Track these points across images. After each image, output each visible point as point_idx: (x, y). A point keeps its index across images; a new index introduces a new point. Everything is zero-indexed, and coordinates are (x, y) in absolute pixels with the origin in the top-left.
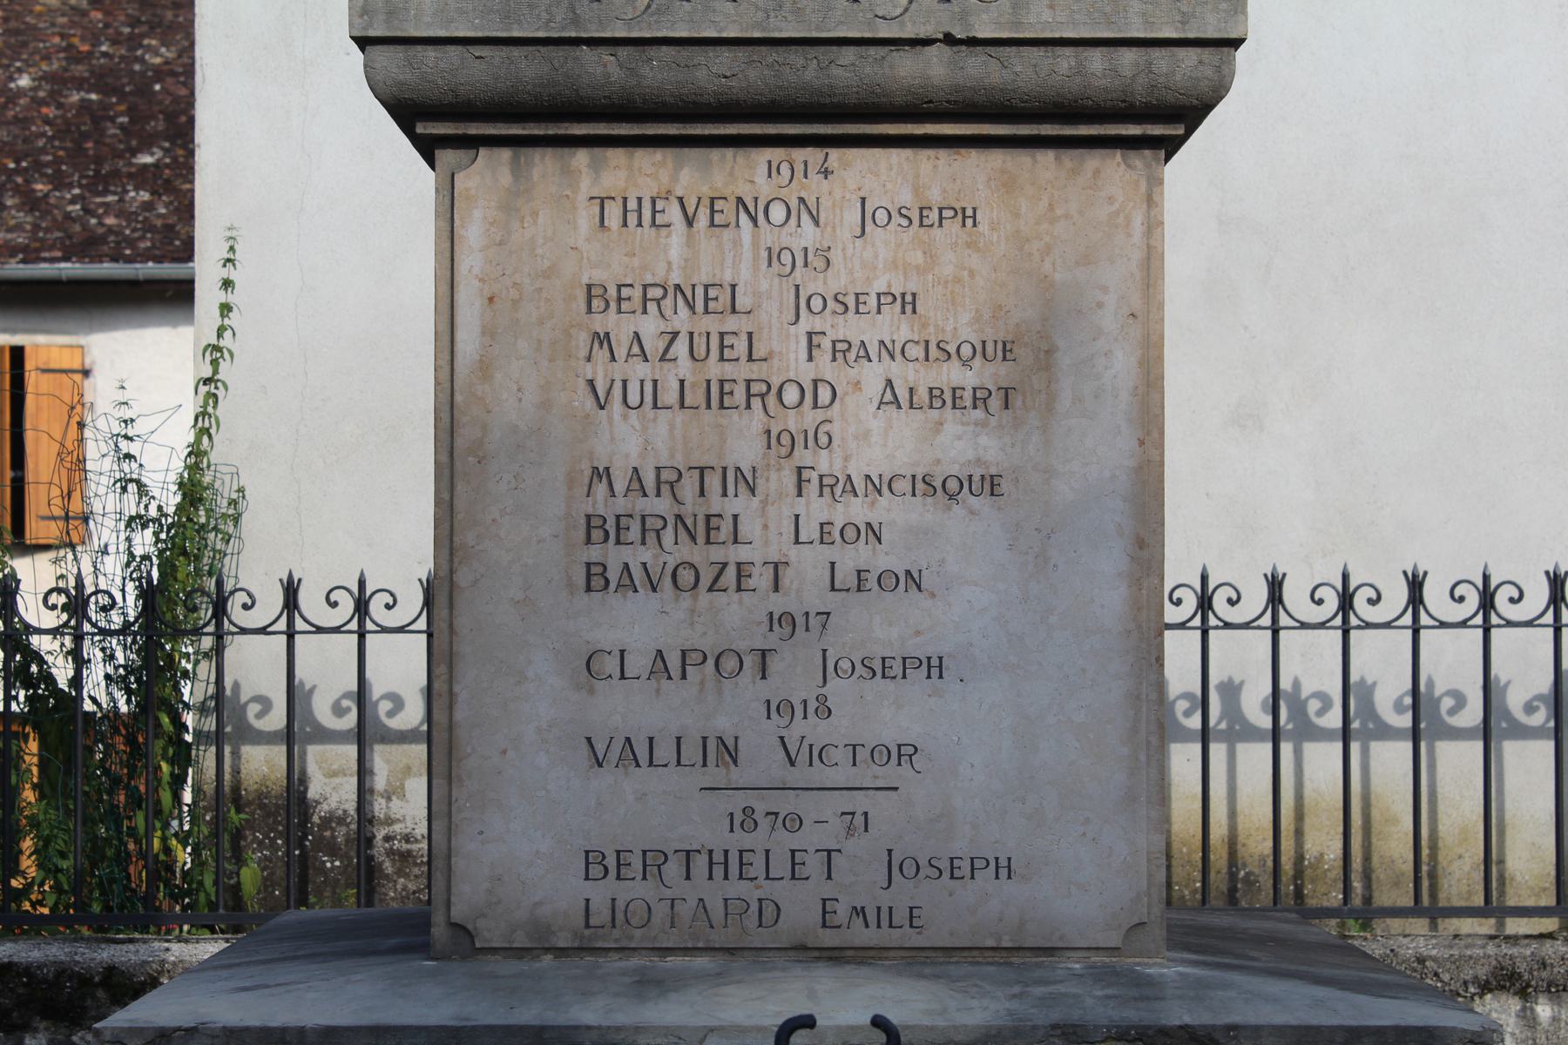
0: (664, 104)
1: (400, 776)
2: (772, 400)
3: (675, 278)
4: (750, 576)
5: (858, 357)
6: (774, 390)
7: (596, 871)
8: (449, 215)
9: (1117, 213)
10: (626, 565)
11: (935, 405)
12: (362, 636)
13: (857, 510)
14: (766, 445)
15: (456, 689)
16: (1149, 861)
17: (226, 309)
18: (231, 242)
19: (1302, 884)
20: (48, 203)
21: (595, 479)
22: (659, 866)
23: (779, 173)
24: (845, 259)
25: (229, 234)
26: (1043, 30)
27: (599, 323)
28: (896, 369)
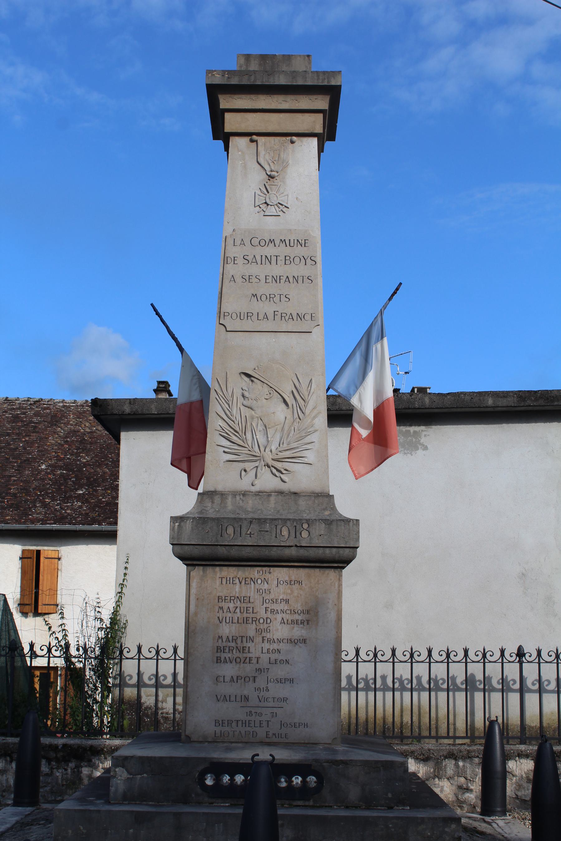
2: (257, 622)
3: (237, 595)
6: (258, 620)
7: (217, 724)
10: (225, 657)
13: (275, 646)
15: (188, 684)
16: (337, 724)
17: (125, 574)
18: (128, 558)
19: (403, 730)
20: (49, 505)
26: (316, 544)
27: (221, 604)
28: (284, 615)
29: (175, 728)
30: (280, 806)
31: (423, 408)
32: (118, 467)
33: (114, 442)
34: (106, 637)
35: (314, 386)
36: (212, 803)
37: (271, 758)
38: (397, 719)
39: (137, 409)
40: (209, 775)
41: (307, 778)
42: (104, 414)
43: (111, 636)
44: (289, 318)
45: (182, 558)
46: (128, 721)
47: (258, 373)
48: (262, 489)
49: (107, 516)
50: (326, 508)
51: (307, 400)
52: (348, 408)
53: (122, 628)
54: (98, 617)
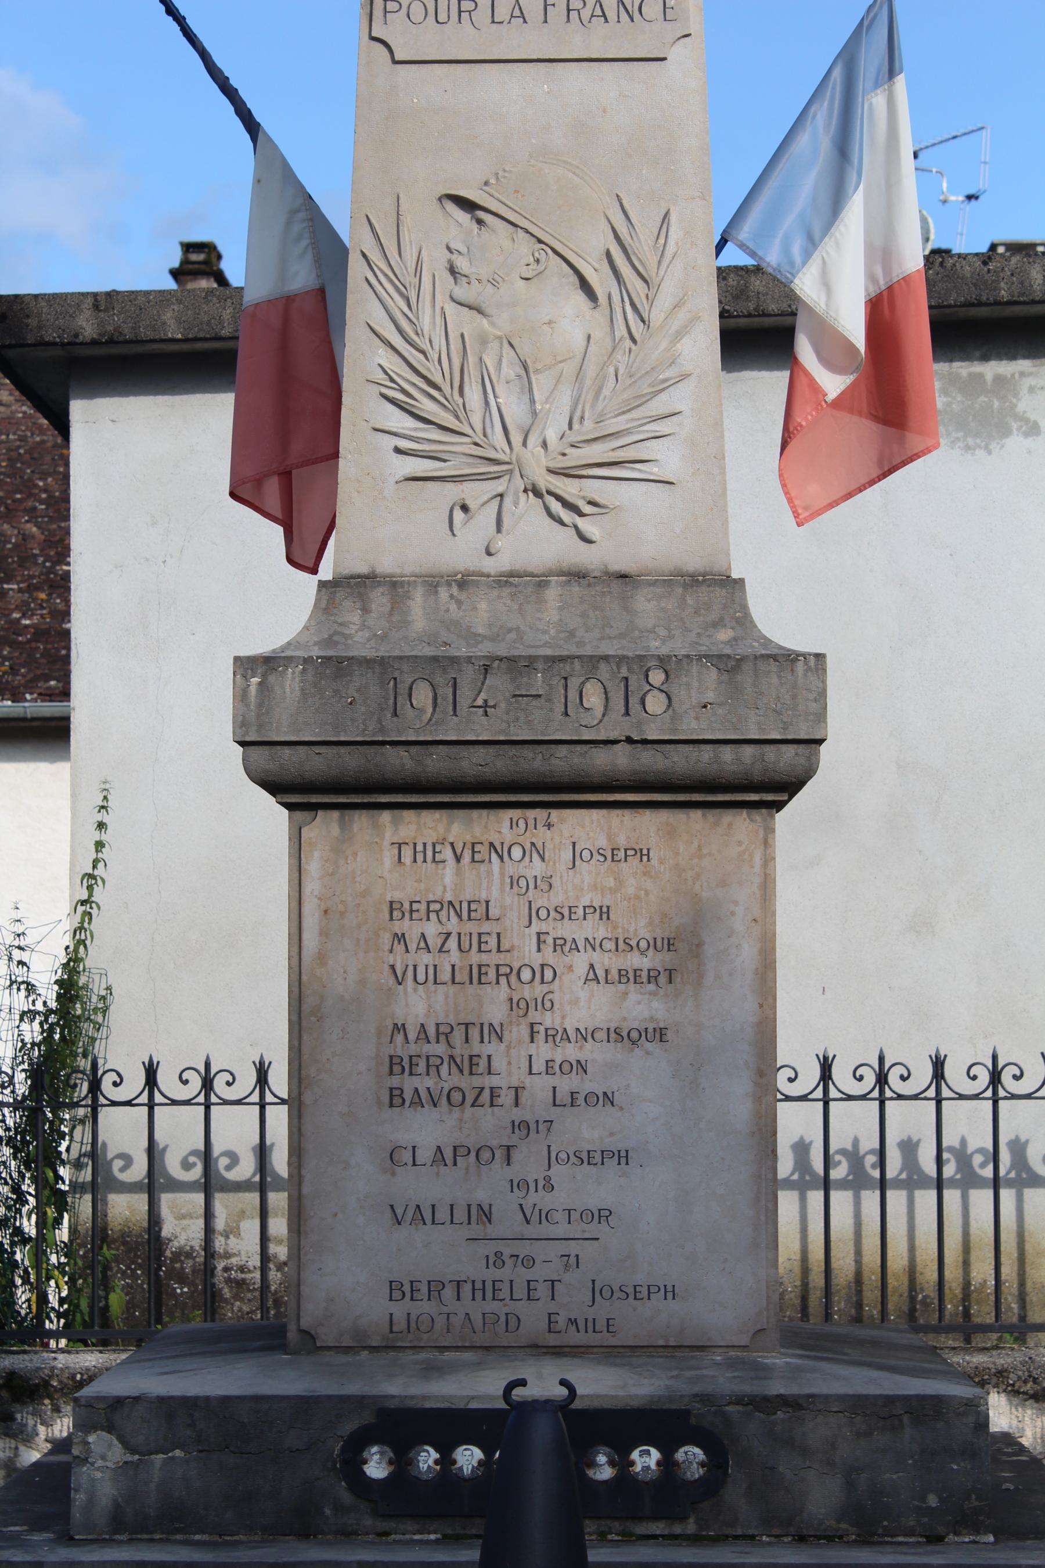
0: (441, 782)
1: (236, 1218)
2: (513, 978)
3: (449, 896)
4: (499, 1096)
5: (571, 949)
6: (515, 972)
7: (397, 1294)
8: (298, 855)
9: (744, 852)
10: (416, 1090)
11: (622, 981)
12: (208, 1107)
13: (570, 1052)
14: (509, 1008)
15: (304, 1172)
16: (767, 1287)
17: (100, 845)
18: (105, 793)
21: (396, 1031)
22: (439, 1291)
23: (517, 826)
24: (562, 883)
25: (104, 786)
26: (691, 734)
27: (398, 927)
28: (596, 957)
29: (268, 1312)
30: (594, 1537)
31: (1024, 303)
32: (67, 518)
33: (52, 436)
34: (48, 1040)
35: (675, 233)
36: (387, 1534)
37: (564, 1391)
38: (953, 1273)
39: (119, 327)
40: (375, 1449)
41: (677, 1451)
42: (14, 342)
43: (63, 1037)
44: (592, 16)
45: (273, 786)
46: (123, 1294)
47: (496, 195)
48: (519, 566)
49: (39, 672)
50: (722, 619)
51: (654, 280)
52: (784, 307)
53: (96, 1010)
54: (20, 979)
